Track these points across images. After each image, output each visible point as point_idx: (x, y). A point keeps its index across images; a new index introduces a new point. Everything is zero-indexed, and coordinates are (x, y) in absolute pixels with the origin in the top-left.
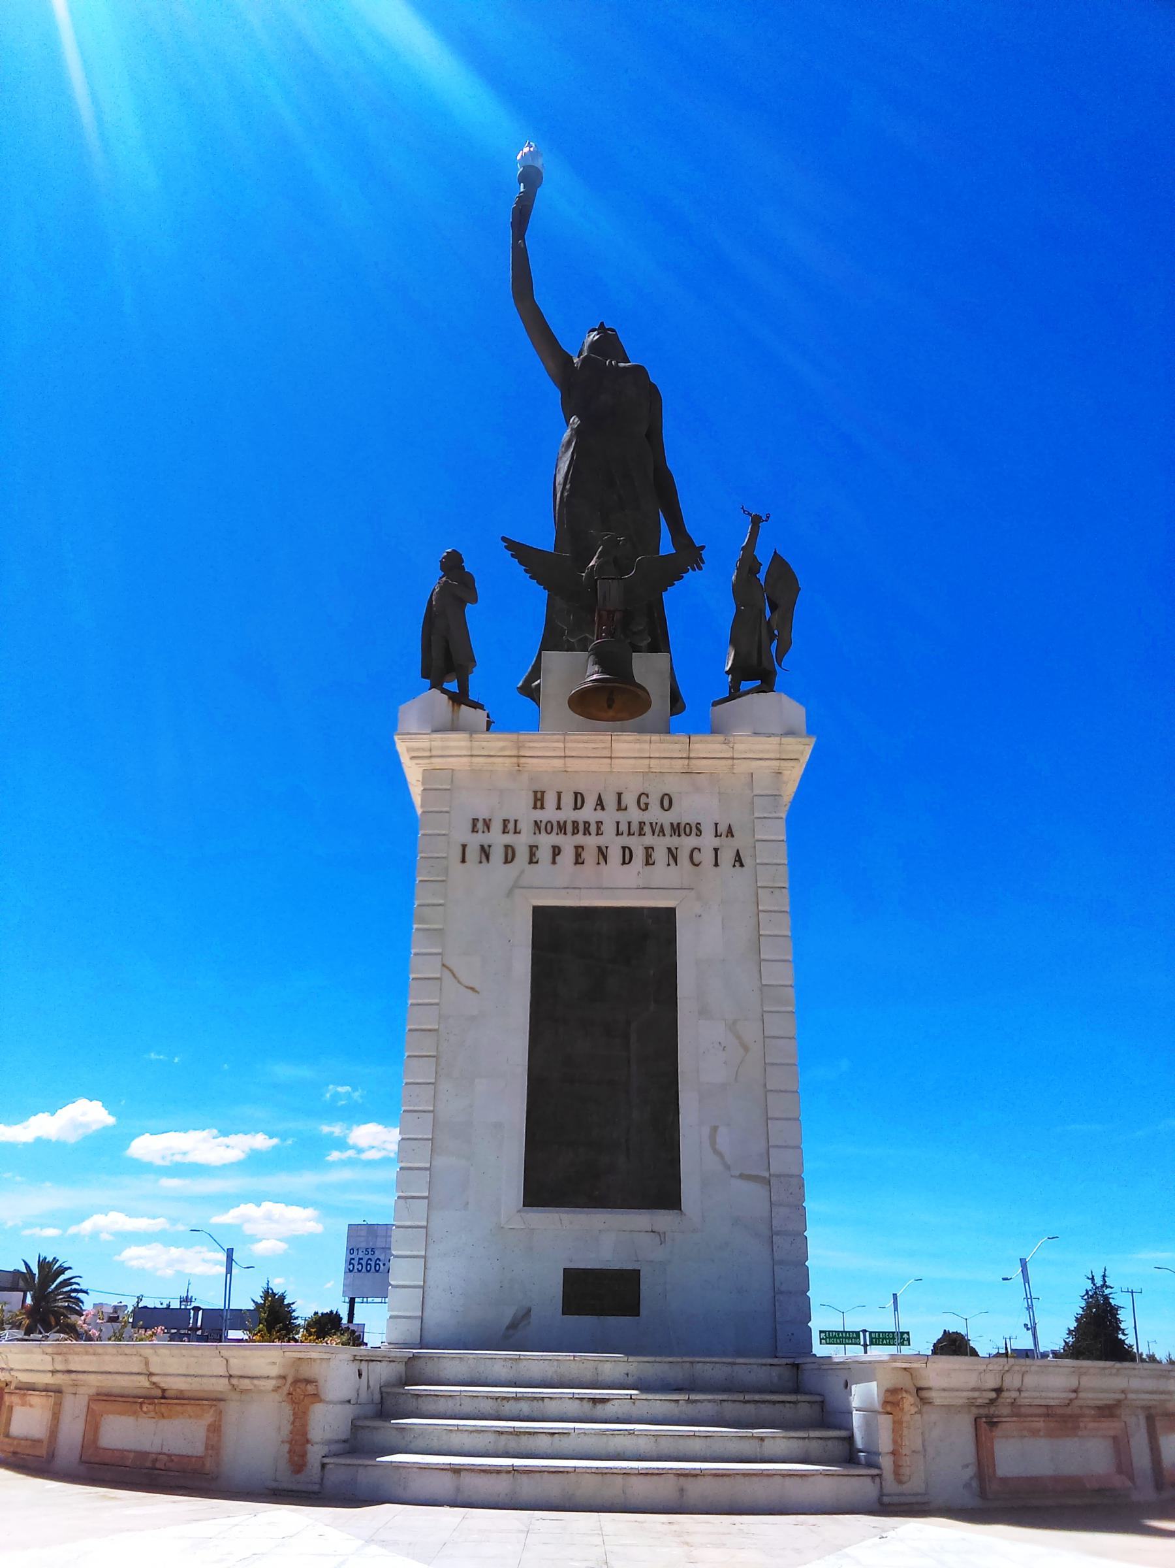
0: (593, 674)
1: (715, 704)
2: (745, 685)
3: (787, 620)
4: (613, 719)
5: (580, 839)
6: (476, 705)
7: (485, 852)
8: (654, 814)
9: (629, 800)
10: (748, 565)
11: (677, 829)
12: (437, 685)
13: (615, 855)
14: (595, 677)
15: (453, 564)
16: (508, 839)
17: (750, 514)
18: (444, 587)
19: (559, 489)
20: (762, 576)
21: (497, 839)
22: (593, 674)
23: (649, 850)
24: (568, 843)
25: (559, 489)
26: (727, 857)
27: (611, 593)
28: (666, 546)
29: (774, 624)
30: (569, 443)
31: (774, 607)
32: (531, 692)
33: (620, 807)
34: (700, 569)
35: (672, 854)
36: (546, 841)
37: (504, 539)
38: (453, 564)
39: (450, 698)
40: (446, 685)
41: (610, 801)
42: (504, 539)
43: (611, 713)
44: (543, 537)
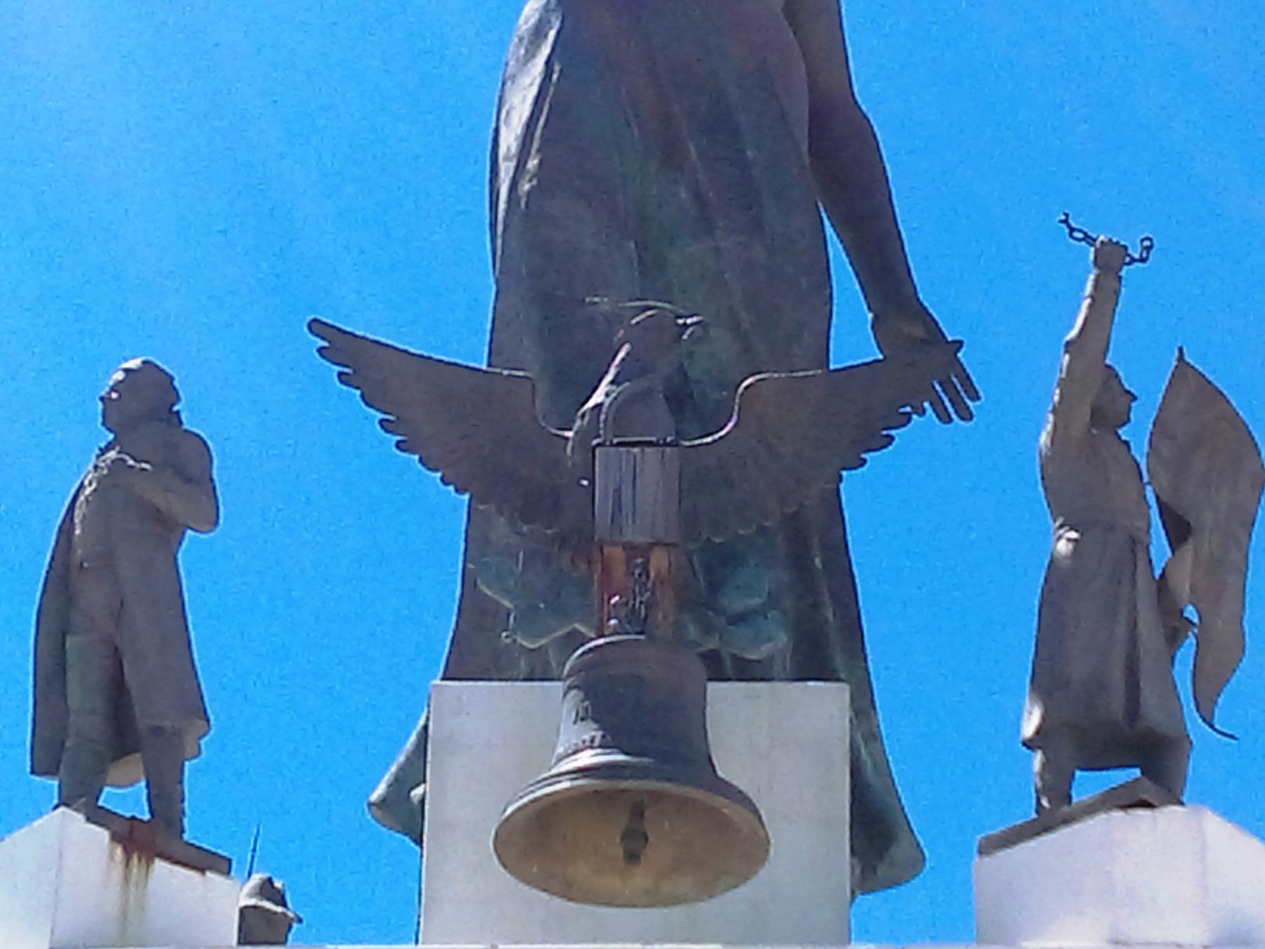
0: (576, 752)
1: (991, 846)
2: (1087, 785)
3: (1226, 576)
4: (653, 899)
6: (204, 861)
10: (1096, 403)
12: (81, 796)
14: (586, 758)
15: (144, 407)
17: (1087, 238)
18: (112, 481)
19: (506, 170)
20: (1137, 433)
22: (576, 752)
25: (506, 170)
27: (638, 490)
28: (853, 337)
29: (1182, 585)
30: (538, 32)
31: (1179, 531)
32: (404, 813)
34: (967, 415)
37: (316, 326)
38: (144, 407)
39: (115, 838)
40: (109, 797)
42: (316, 326)
43: (640, 879)
44: (452, 313)
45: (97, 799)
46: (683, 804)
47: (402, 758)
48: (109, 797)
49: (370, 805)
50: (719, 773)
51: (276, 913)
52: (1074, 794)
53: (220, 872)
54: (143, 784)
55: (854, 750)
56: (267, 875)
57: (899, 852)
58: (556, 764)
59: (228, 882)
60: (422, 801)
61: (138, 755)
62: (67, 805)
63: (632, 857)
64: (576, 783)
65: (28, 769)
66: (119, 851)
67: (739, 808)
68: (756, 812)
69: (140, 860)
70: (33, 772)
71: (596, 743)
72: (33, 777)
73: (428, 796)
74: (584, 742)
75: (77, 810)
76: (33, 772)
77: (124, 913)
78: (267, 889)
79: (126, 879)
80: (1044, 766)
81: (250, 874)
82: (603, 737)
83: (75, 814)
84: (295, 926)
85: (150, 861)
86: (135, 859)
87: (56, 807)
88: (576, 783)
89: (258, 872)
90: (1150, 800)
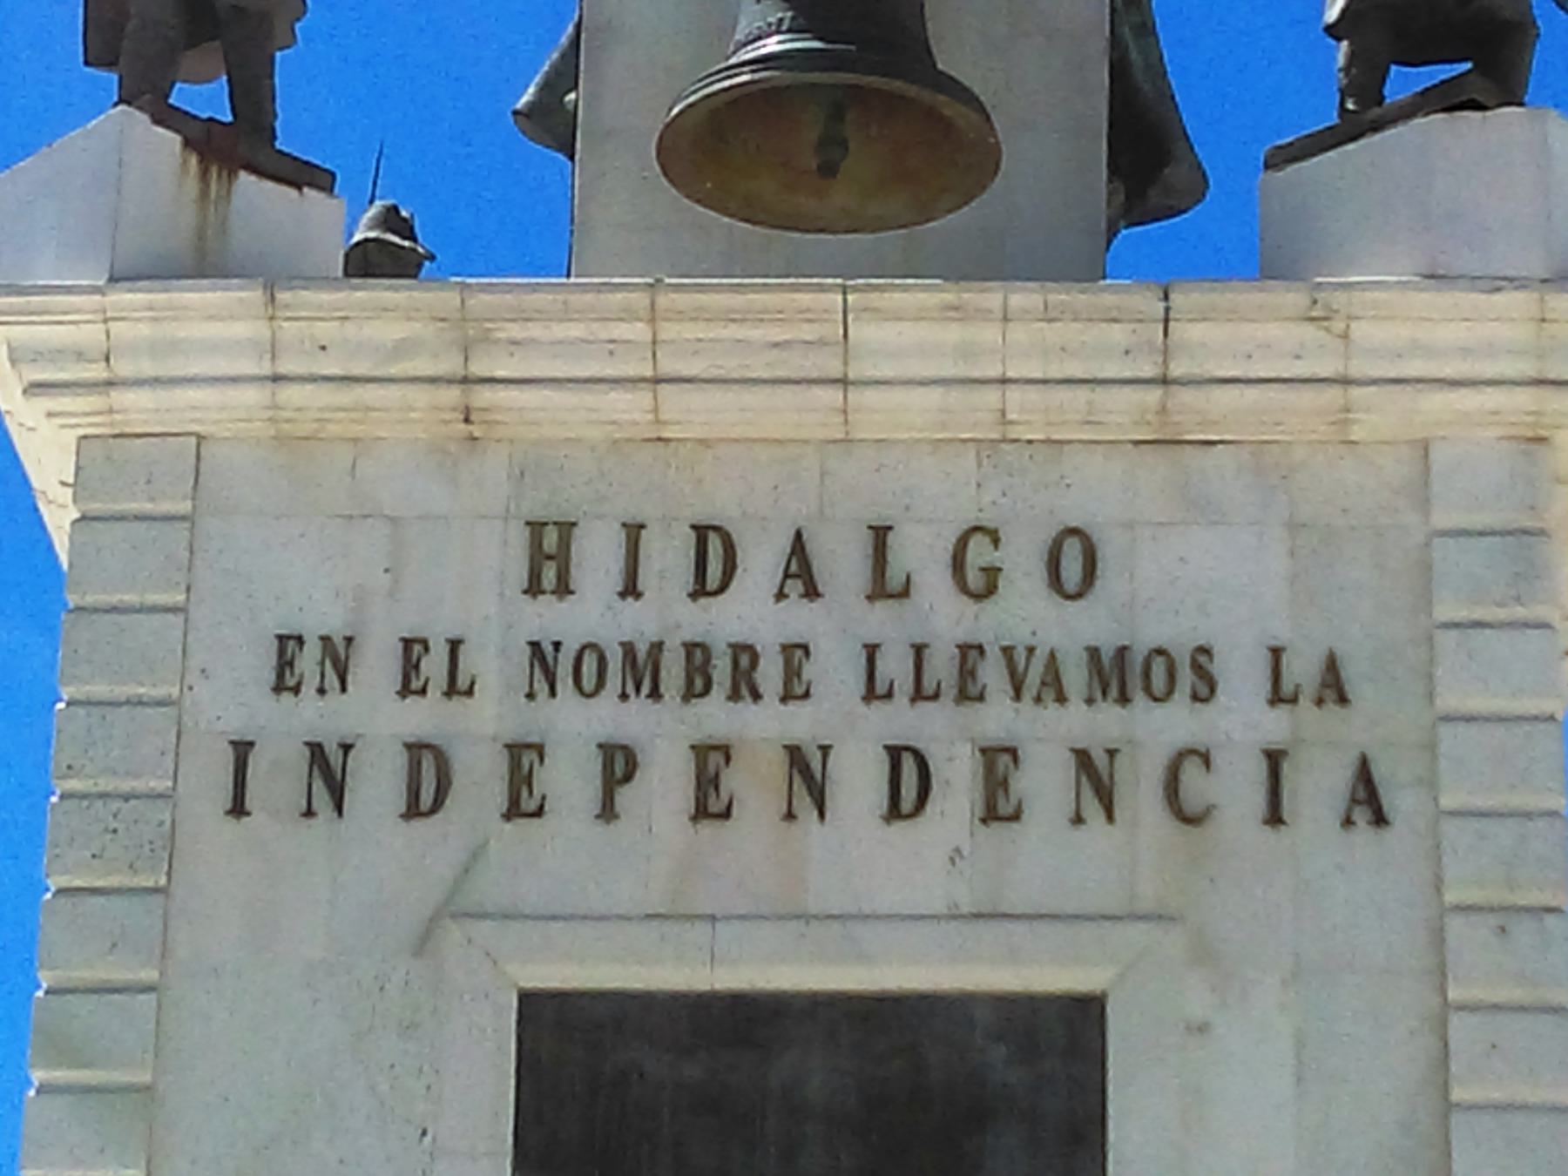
1: (1281, 158)
2: (1402, 82)
5: (716, 716)
6: (302, 175)
7: (328, 770)
8: (1026, 612)
9: (921, 554)
11: (1115, 675)
12: (148, 93)
13: (858, 780)
14: (772, 45)
16: (424, 717)
21: (375, 716)
23: (998, 762)
24: (665, 732)
26: (1318, 786)
32: (552, 123)
33: (884, 586)
35: (1095, 777)
36: (576, 725)
39: (187, 143)
40: (182, 96)
41: (841, 562)
43: (841, 195)
45: (167, 96)
46: (894, 103)
47: (555, 56)
48: (182, 96)
49: (516, 113)
50: (940, 66)
51: (403, 248)
52: (1386, 92)
53: (321, 188)
54: (225, 78)
55: (1115, 41)
56: (389, 202)
57: (1174, 174)
58: (734, 53)
59: (335, 201)
60: (576, 107)
61: (217, 44)
62: (129, 103)
63: (828, 170)
64: (757, 76)
65: (81, 59)
66: (194, 160)
67: (963, 109)
68: (981, 109)
69: (219, 175)
70: (87, 63)
71: (784, 28)
72: (88, 69)
73: (581, 103)
74: (770, 25)
75: (140, 108)
76: (87, 63)
77: (201, 235)
78: (392, 219)
79: (204, 193)
80: (1352, 57)
81: (371, 202)
82: (793, 19)
83: (137, 113)
84: (427, 263)
85: (232, 175)
86: (214, 170)
87: (116, 104)
88: (757, 76)
89: (381, 198)
90: (1480, 99)
